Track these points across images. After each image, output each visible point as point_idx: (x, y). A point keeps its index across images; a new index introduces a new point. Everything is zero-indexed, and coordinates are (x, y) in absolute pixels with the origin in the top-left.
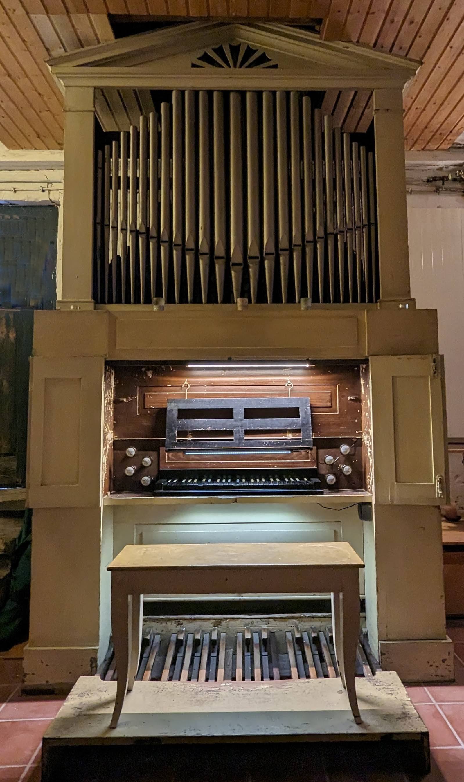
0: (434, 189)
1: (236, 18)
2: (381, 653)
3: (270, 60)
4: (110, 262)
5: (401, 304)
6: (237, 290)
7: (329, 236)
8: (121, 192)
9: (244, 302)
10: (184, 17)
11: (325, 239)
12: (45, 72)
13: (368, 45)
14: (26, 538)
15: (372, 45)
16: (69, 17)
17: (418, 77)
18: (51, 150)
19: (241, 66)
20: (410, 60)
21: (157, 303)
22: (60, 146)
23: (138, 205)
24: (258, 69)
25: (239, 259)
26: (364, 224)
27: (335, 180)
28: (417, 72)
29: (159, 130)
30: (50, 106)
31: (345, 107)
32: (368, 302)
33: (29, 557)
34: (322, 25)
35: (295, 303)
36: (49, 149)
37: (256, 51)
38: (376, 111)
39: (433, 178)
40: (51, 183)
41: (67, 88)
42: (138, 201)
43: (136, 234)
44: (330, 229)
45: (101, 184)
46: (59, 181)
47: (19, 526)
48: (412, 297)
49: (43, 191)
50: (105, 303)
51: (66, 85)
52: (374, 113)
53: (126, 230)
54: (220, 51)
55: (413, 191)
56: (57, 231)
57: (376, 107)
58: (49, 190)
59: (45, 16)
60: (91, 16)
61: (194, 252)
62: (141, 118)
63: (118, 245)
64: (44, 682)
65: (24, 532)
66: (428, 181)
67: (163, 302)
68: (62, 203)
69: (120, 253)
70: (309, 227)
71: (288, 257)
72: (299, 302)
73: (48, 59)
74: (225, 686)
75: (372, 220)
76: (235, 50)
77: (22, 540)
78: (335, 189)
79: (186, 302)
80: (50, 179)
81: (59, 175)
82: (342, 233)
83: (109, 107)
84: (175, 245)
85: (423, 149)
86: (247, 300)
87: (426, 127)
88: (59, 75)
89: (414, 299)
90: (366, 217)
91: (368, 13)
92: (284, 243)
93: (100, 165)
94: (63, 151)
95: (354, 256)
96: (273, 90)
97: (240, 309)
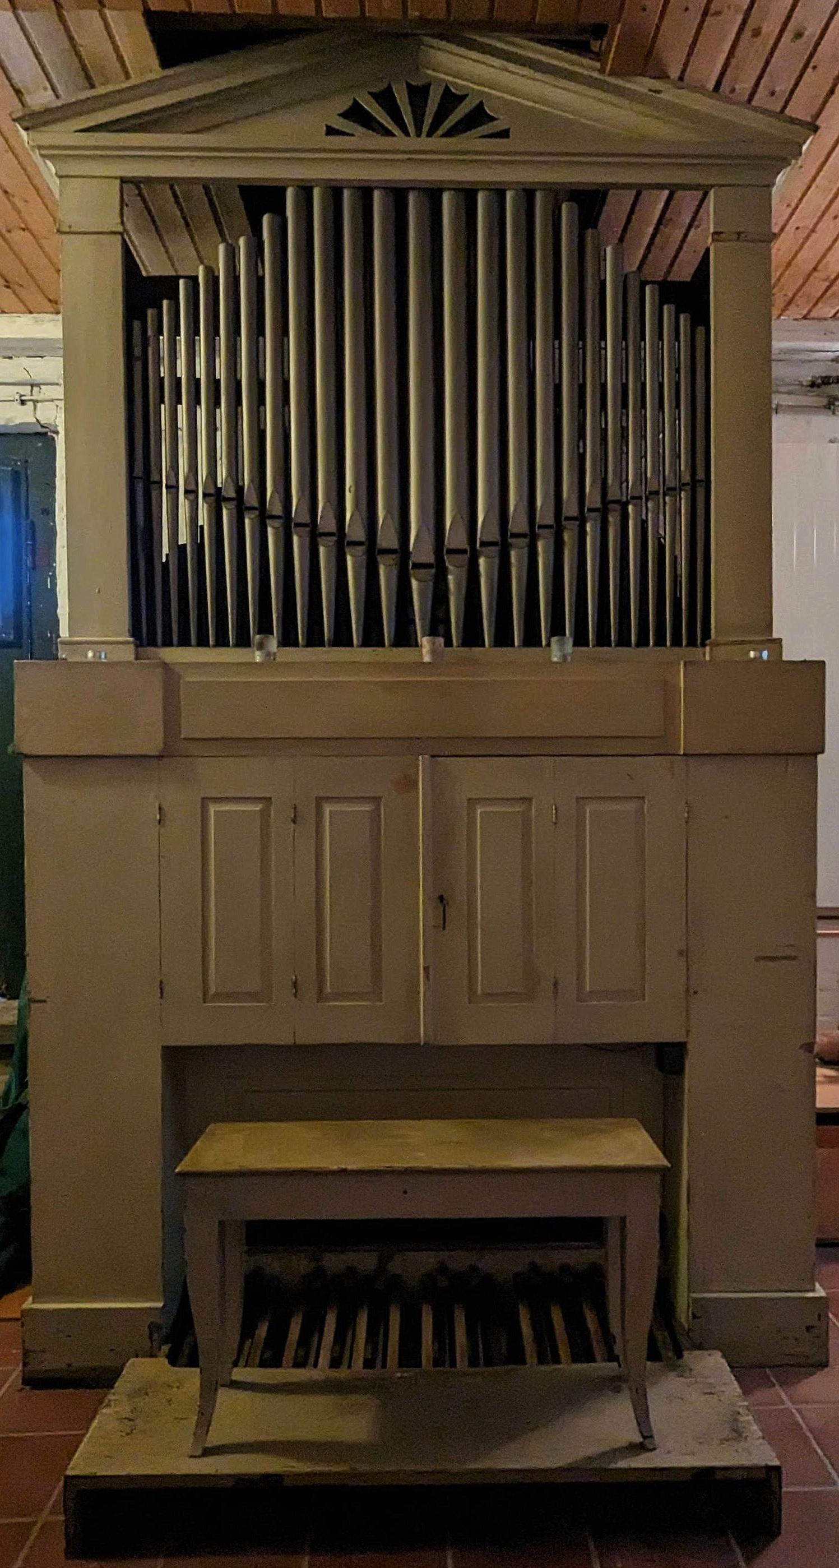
0: (824, 401)
1: (423, 21)
2: (693, 1313)
3: (492, 119)
4: (164, 560)
5: (754, 650)
6: (422, 619)
7: (611, 506)
8: (182, 410)
9: (437, 644)
10: (306, 19)
11: (604, 512)
12: (13, 142)
13: (703, 87)
14: (17, 1098)
15: (711, 86)
16: (61, 18)
17: (805, 159)
18: (35, 315)
19: (429, 134)
20: (792, 121)
21: (261, 646)
22: (54, 305)
23: (218, 433)
24: (471, 141)
25: (427, 556)
26: (683, 481)
27: (625, 387)
28: (805, 147)
29: (260, 273)
30: (27, 218)
31: (648, 226)
32: (688, 645)
33: (25, 1133)
34: (606, 39)
35: (540, 645)
36: (31, 313)
37: (464, 97)
38: (716, 236)
39: (822, 378)
40: (38, 385)
41: (64, 180)
42: (218, 425)
43: (216, 498)
44: (613, 494)
45: (142, 396)
46: (56, 381)
47: (6, 1074)
48: (775, 635)
49: (23, 402)
50: (156, 645)
51: (61, 173)
52: (710, 239)
53: (196, 492)
54: (386, 99)
55: (781, 406)
56: (55, 488)
57: (715, 227)
58: (35, 402)
59: (10, 14)
60: (108, 12)
61: (335, 538)
62: (221, 248)
63: (182, 521)
64: (64, 1366)
65: (13, 1087)
66: (813, 385)
67: (273, 643)
68: (61, 429)
69: (183, 538)
70: (570, 489)
71: (526, 550)
72: (549, 645)
73: (19, 114)
74: (401, 1377)
75: (700, 475)
76: (418, 94)
77: (11, 1101)
78: (625, 405)
79: (321, 644)
80: (37, 378)
81: (52, 368)
82: (638, 501)
83: (154, 222)
84: (297, 525)
85: (805, 317)
86: (441, 640)
87: (815, 269)
88: (43, 152)
89: (780, 640)
90: (686, 466)
91: (705, 14)
92: (518, 522)
93: (137, 352)
94: (60, 317)
95: (661, 549)
96: (498, 187)
97: (427, 659)
